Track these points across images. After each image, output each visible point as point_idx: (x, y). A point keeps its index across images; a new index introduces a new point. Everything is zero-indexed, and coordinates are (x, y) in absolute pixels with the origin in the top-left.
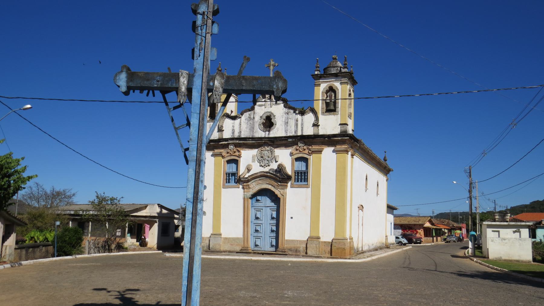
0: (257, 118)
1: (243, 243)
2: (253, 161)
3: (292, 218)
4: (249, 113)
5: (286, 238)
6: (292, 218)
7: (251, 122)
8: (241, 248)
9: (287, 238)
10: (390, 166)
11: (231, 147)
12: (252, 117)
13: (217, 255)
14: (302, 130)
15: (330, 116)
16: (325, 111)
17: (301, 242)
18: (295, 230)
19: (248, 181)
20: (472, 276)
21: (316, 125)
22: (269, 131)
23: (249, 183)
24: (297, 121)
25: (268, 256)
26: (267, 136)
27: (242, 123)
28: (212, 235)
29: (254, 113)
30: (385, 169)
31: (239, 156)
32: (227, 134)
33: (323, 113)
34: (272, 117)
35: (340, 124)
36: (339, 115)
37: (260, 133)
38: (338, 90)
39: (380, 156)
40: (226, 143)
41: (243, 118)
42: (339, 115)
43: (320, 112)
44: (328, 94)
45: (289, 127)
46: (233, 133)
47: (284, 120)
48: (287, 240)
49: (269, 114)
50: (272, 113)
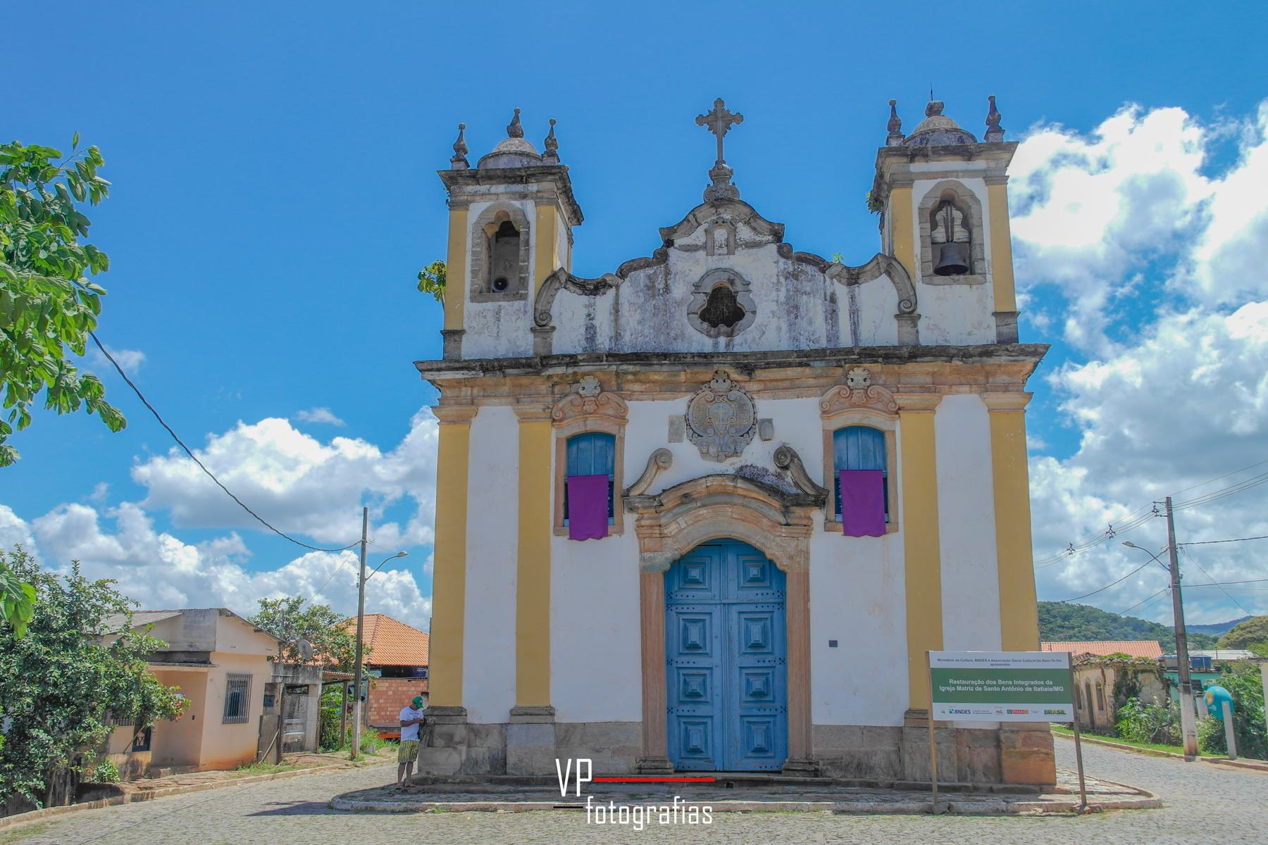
0: (680, 290)
1: (640, 745)
2: (674, 436)
3: (833, 644)
4: (650, 271)
5: (817, 720)
6: (833, 644)
7: (658, 301)
8: (633, 764)
9: (821, 716)
10: (202, 646)
12: (660, 285)
14: (855, 333)
15: (956, 288)
16: (931, 271)
17: (873, 732)
20: (329, 808)
21: (908, 313)
22: (730, 335)
24: (833, 300)
25: (745, 791)
26: (722, 349)
27: (625, 309)
28: (514, 713)
29: (667, 273)
31: (622, 419)
32: (566, 339)
34: (739, 286)
35: (995, 314)
36: (989, 286)
37: (697, 339)
38: (978, 202)
39: (358, 590)
41: (626, 288)
42: (989, 286)
43: (918, 274)
45: (803, 323)
47: (782, 299)
48: (818, 727)
49: (723, 279)
50: (736, 274)
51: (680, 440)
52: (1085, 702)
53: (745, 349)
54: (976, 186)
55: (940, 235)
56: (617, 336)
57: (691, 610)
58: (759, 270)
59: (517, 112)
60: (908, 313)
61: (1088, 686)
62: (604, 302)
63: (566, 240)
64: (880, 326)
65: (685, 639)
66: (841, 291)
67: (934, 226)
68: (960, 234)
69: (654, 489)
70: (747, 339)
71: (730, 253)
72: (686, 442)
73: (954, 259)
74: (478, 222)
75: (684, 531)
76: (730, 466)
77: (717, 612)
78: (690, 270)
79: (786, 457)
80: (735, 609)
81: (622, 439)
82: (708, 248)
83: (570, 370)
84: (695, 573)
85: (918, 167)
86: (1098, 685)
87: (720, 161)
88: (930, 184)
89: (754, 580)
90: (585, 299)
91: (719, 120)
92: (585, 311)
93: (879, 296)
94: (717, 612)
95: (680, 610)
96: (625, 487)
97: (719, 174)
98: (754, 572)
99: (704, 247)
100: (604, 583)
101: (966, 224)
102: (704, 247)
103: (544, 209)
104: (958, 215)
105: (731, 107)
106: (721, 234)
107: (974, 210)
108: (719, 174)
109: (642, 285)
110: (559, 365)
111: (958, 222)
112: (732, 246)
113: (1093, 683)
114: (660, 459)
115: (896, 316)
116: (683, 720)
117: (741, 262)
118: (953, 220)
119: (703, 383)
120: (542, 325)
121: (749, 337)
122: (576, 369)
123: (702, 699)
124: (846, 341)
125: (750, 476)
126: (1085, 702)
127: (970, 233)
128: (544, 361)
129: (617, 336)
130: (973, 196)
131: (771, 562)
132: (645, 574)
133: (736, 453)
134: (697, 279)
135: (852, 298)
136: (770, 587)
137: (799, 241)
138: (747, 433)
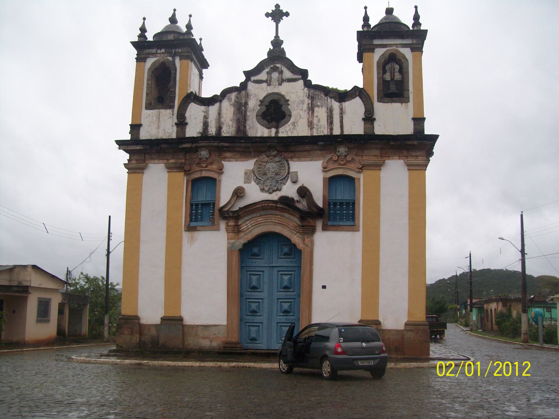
2: (247, 180)
3: (324, 287)
6: (324, 287)
21: (369, 118)
22: (277, 127)
26: (273, 135)
31: (220, 171)
33: (380, 100)
36: (411, 104)
38: (407, 60)
40: (194, 145)
46: (173, 20)
51: (249, 183)
52: (490, 319)
53: (285, 135)
54: (407, 52)
55: (388, 77)
56: (219, 129)
57: (253, 270)
58: (294, 92)
59: (175, 10)
60: (369, 118)
61: (491, 310)
62: (213, 110)
63: (198, 76)
64: (354, 126)
65: (250, 283)
66: (336, 105)
67: (384, 72)
68: (398, 77)
69: (236, 208)
70: (285, 131)
71: (280, 84)
72: (253, 183)
73: (393, 88)
74: (150, 68)
75: (252, 228)
76: (275, 196)
77: (267, 271)
78: (258, 93)
79: (304, 192)
80: (276, 270)
81: (220, 181)
82: (268, 82)
83: (194, 145)
84: (255, 250)
85: (376, 42)
86: (495, 309)
87: (277, 36)
88: (384, 50)
89: (286, 254)
90: (203, 108)
91: (277, 15)
92: (203, 114)
93: (355, 108)
94: (267, 271)
95: (248, 269)
96: (222, 205)
97: (277, 43)
98: (286, 250)
99: (266, 81)
100: (210, 254)
101: (401, 71)
102: (266, 81)
103: (185, 62)
104: (397, 67)
105: (284, 9)
106: (275, 75)
107: (404, 65)
108: (277, 43)
109: (233, 100)
110: (188, 143)
111: (397, 70)
112: (281, 81)
113: (493, 309)
114: (239, 193)
115: (363, 119)
116: (248, 324)
117: (285, 89)
118: (394, 69)
119: (263, 152)
120: (182, 123)
121: (287, 129)
122: (197, 145)
123: (258, 314)
124: (337, 131)
125: (286, 202)
126: (490, 319)
127: (403, 76)
128: (181, 139)
129: (219, 129)
130: (404, 57)
131: (295, 245)
132: (230, 251)
133: (279, 190)
134: (261, 98)
135: (341, 109)
136: (294, 258)
137: (315, 79)
138: (285, 179)
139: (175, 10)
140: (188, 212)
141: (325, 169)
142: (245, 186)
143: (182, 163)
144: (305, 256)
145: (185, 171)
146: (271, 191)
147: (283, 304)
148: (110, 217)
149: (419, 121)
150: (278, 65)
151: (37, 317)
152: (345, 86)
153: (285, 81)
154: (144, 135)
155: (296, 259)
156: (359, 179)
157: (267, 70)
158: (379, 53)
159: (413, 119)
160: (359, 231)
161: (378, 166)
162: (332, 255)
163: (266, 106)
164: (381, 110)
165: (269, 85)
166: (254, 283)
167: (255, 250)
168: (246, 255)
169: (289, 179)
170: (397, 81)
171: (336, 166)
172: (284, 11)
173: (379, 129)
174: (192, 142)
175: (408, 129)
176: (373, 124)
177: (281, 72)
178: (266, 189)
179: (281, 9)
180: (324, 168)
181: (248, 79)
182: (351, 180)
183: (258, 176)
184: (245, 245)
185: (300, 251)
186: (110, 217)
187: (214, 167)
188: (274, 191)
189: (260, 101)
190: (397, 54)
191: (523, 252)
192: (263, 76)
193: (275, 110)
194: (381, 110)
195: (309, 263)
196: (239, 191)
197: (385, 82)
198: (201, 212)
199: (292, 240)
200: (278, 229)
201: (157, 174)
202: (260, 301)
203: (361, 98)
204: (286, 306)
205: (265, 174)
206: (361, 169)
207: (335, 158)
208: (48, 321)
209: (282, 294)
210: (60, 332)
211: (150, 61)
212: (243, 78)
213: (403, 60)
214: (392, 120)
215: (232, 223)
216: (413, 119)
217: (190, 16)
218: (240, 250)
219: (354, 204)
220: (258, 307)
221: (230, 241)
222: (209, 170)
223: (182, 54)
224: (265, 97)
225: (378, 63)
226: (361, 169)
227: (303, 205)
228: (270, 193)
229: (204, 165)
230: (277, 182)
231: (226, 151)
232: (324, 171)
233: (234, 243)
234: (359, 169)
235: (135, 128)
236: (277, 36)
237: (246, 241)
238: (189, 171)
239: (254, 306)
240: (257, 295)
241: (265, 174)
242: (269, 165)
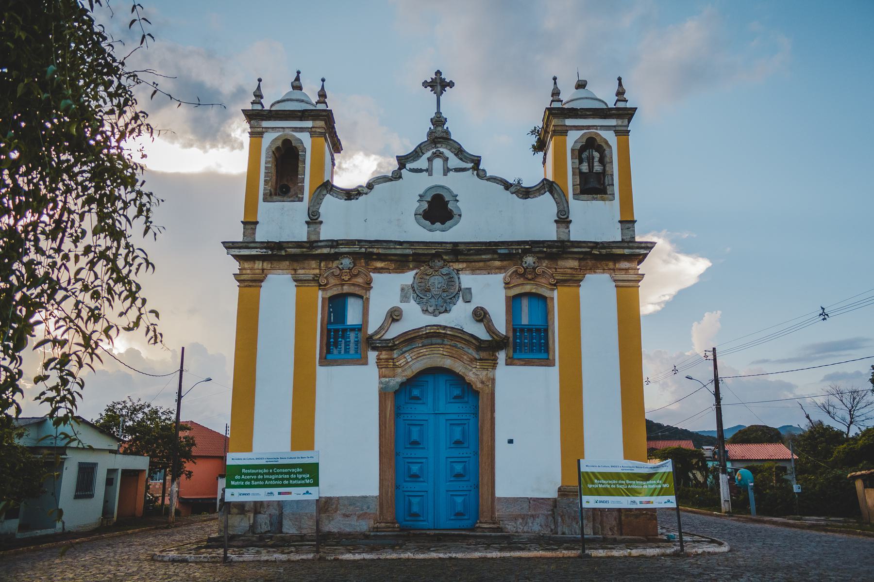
2: (404, 298)
3: (511, 441)
6: (511, 441)
11: (346, 262)
13: (448, 549)
18: (525, 466)
19: (390, 346)
21: (563, 220)
23: (395, 354)
30: (579, 461)
33: (576, 196)
40: (333, 251)
44: (584, 155)
46: (297, 86)
48: (499, 498)
51: (408, 302)
54: (610, 137)
55: (585, 168)
58: (461, 186)
60: (563, 220)
68: (597, 168)
71: (445, 174)
73: (593, 184)
74: (270, 147)
75: (413, 362)
79: (481, 315)
80: (442, 419)
82: (429, 171)
84: (416, 392)
87: (438, 113)
89: (456, 397)
91: (439, 84)
97: (439, 121)
99: (427, 170)
100: (352, 397)
101: (602, 161)
102: (427, 170)
106: (438, 163)
108: (439, 121)
111: (596, 159)
114: (394, 316)
118: (593, 158)
119: (424, 262)
123: (421, 479)
132: (383, 394)
136: (467, 402)
139: (299, 73)
140: (325, 341)
141: (507, 285)
142: (403, 306)
143: (315, 275)
144: (483, 401)
145: (320, 285)
146: (437, 312)
147: (454, 464)
148: (183, 348)
149: (628, 223)
150: (441, 150)
151: (77, 491)
152: (531, 180)
153: (451, 170)
154: (261, 235)
155: (475, 403)
156: (553, 299)
157: (429, 154)
158: (573, 138)
159: (620, 222)
160: (554, 365)
161: (574, 281)
162: (522, 397)
163: (428, 202)
164: (578, 208)
165: (430, 175)
166: (415, 437)
167: (416, 392)
168: (398, 400)
169: (461, 298)
170: (598, 174)
171: (521, 281)
172: (448, 80)
173: (577, 233)
174: (331, 247)
175: (615, 235)
176: (568, 227)
177: (446, 160)
178: (431, 309)
179: (443, 77)
180: (506, 284)
181: (402, 166)
182: (544, 298)
183: (420, 293)
184: (402, 384)
185: (476, 393)
186: (183, 348)
187: (360, 280)
188: (440, 313)
189: (420, 196)
190: (598, 139)
191: (717, 394)
192: (422, 163)
193: (438, 209)
194: (578, 208)
195: (489, 409)
196: (396, 313)
197: (581, 173)
198: (337, 340)
199: (466, 378)
200: (448, 363)
201: (280, 290)
202: (423, 460)
203: (551, 193)
204: (459, 468)
205: (429, 290)
206: (555, 285)
207: (521, 271)
208: (91, 496)
209: (456, 453)
210: (107, 511)
211: (268, 139)
212: (395, 165)
213: (605, 146)
214: (593, 221)
215: (384, 355)
216: (620, 222)
217: (323, 80)
218: (396, 392)
219: (546, 331)
220: (421, 469)
221: (384, 380)
222: (353, 285)
223: (314, 130)
224: (426, 191)
225: (573, 150)
226: (554, 286)
227: (480, 331)
228: (435, 316)
229: (346, 278)
230: (445, 302)
231: (375, 260)
232: (505, 288)
233: (389, 382)
234: (551, 284)
235: (250, 225)
236: (438, 113)
237: (405, 379)
238: (325, 285)
239: (415, 469)
240: (418, 453)
241: (429, 290)
242: (432, 280)
